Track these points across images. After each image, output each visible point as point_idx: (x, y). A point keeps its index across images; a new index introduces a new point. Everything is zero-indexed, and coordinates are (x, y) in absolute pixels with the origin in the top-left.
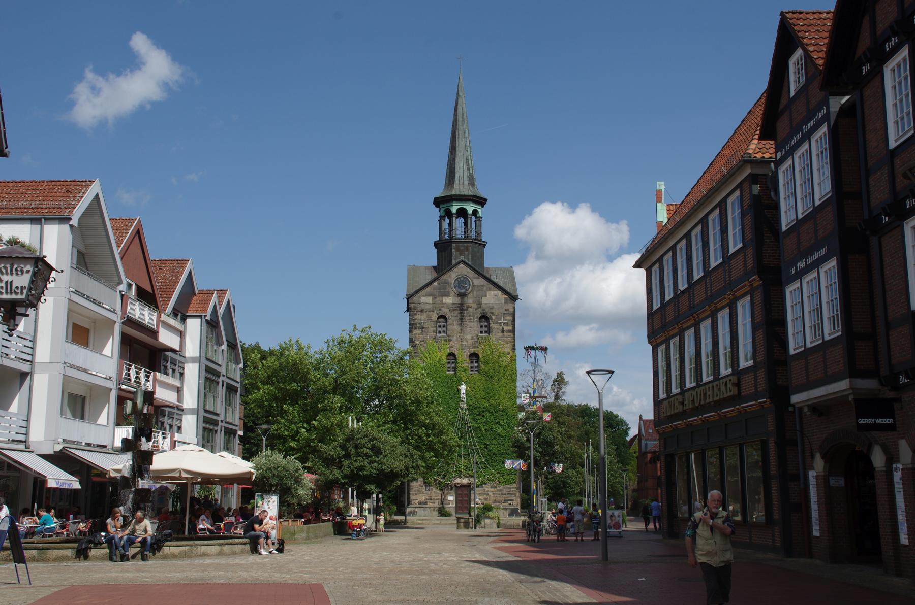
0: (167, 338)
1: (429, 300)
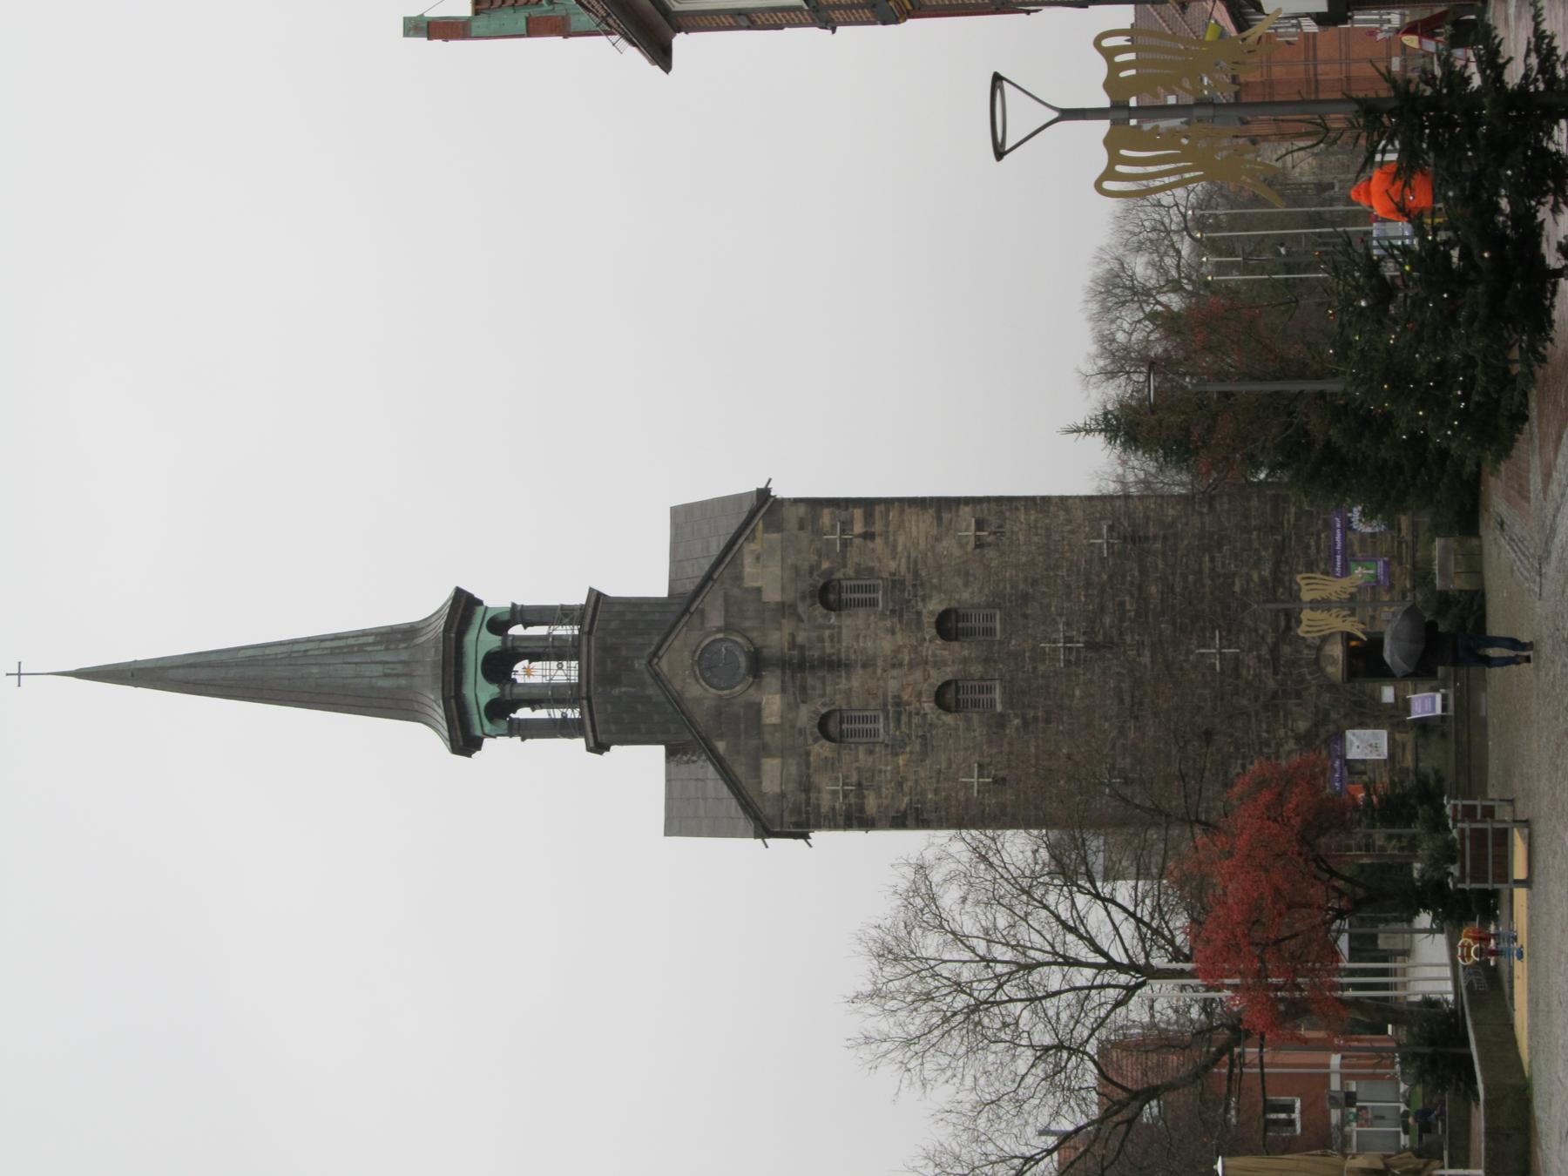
1: (771, 766)
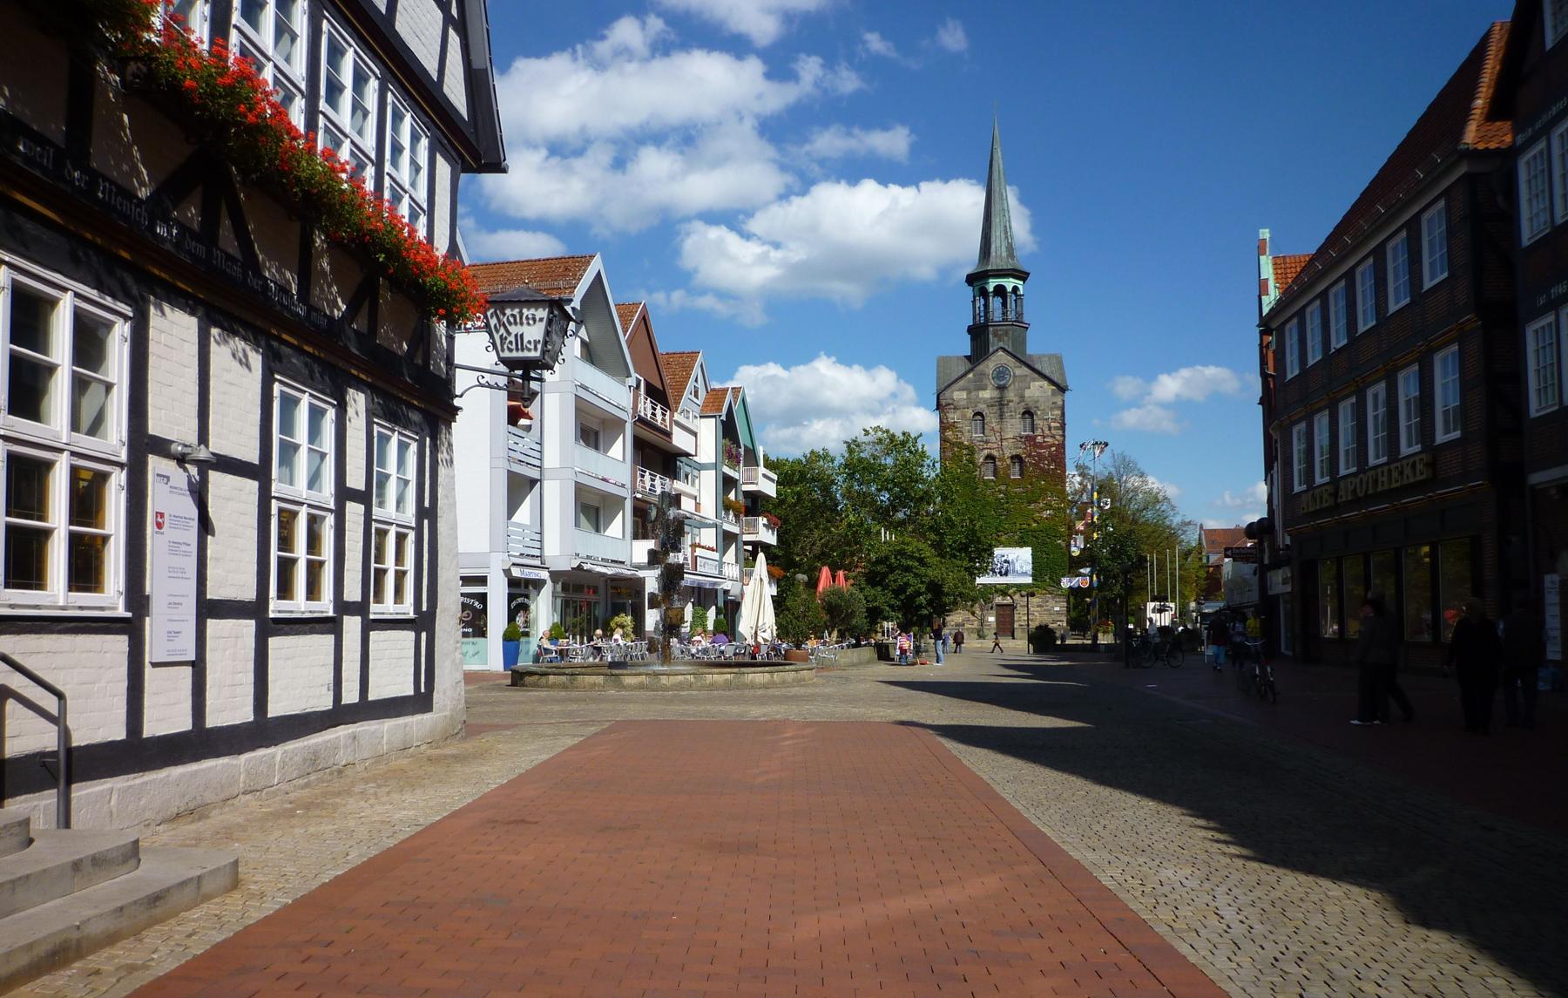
0: (680, 440)
1: (964, 395)
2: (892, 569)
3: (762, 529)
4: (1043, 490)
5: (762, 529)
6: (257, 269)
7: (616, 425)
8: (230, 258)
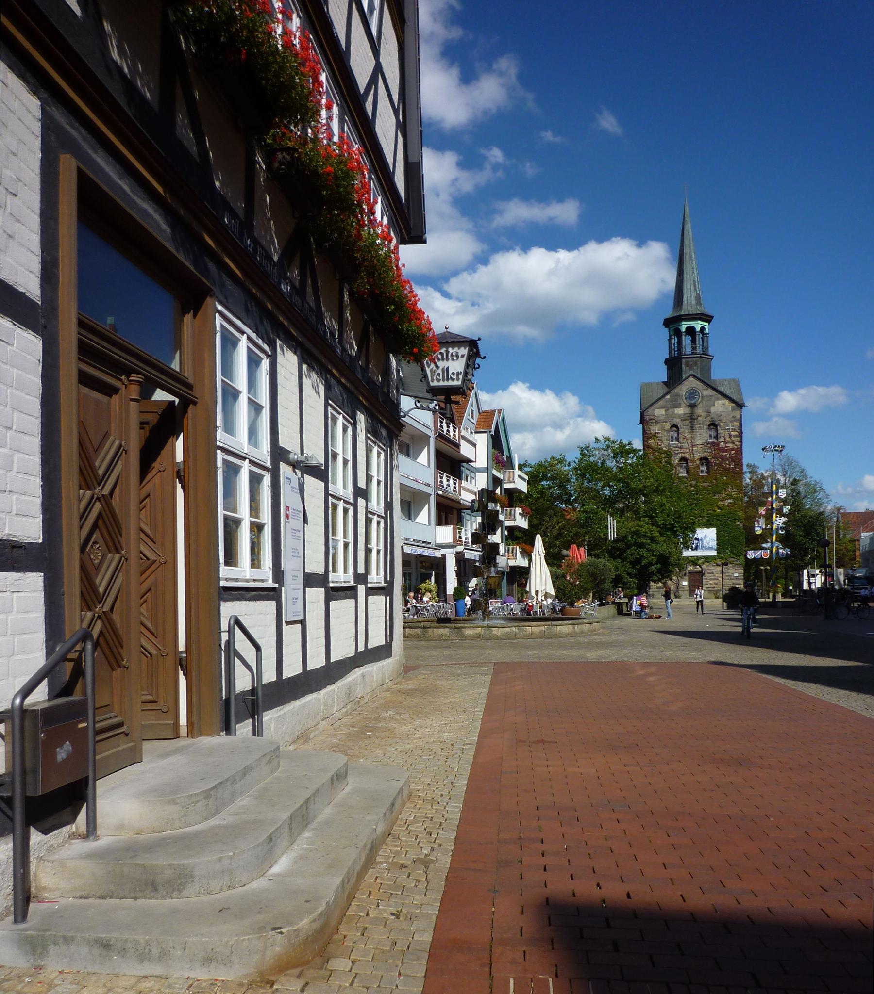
0: (465, 450)
1: (663, 412)
2: (629, 547)
3: (518, 517)
4: (726, 484)
5: (518, 517)
6: (320, 317)
7: (423, 439)
8: (311, 309)
